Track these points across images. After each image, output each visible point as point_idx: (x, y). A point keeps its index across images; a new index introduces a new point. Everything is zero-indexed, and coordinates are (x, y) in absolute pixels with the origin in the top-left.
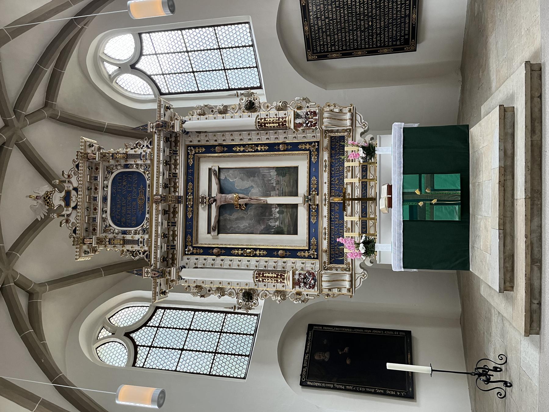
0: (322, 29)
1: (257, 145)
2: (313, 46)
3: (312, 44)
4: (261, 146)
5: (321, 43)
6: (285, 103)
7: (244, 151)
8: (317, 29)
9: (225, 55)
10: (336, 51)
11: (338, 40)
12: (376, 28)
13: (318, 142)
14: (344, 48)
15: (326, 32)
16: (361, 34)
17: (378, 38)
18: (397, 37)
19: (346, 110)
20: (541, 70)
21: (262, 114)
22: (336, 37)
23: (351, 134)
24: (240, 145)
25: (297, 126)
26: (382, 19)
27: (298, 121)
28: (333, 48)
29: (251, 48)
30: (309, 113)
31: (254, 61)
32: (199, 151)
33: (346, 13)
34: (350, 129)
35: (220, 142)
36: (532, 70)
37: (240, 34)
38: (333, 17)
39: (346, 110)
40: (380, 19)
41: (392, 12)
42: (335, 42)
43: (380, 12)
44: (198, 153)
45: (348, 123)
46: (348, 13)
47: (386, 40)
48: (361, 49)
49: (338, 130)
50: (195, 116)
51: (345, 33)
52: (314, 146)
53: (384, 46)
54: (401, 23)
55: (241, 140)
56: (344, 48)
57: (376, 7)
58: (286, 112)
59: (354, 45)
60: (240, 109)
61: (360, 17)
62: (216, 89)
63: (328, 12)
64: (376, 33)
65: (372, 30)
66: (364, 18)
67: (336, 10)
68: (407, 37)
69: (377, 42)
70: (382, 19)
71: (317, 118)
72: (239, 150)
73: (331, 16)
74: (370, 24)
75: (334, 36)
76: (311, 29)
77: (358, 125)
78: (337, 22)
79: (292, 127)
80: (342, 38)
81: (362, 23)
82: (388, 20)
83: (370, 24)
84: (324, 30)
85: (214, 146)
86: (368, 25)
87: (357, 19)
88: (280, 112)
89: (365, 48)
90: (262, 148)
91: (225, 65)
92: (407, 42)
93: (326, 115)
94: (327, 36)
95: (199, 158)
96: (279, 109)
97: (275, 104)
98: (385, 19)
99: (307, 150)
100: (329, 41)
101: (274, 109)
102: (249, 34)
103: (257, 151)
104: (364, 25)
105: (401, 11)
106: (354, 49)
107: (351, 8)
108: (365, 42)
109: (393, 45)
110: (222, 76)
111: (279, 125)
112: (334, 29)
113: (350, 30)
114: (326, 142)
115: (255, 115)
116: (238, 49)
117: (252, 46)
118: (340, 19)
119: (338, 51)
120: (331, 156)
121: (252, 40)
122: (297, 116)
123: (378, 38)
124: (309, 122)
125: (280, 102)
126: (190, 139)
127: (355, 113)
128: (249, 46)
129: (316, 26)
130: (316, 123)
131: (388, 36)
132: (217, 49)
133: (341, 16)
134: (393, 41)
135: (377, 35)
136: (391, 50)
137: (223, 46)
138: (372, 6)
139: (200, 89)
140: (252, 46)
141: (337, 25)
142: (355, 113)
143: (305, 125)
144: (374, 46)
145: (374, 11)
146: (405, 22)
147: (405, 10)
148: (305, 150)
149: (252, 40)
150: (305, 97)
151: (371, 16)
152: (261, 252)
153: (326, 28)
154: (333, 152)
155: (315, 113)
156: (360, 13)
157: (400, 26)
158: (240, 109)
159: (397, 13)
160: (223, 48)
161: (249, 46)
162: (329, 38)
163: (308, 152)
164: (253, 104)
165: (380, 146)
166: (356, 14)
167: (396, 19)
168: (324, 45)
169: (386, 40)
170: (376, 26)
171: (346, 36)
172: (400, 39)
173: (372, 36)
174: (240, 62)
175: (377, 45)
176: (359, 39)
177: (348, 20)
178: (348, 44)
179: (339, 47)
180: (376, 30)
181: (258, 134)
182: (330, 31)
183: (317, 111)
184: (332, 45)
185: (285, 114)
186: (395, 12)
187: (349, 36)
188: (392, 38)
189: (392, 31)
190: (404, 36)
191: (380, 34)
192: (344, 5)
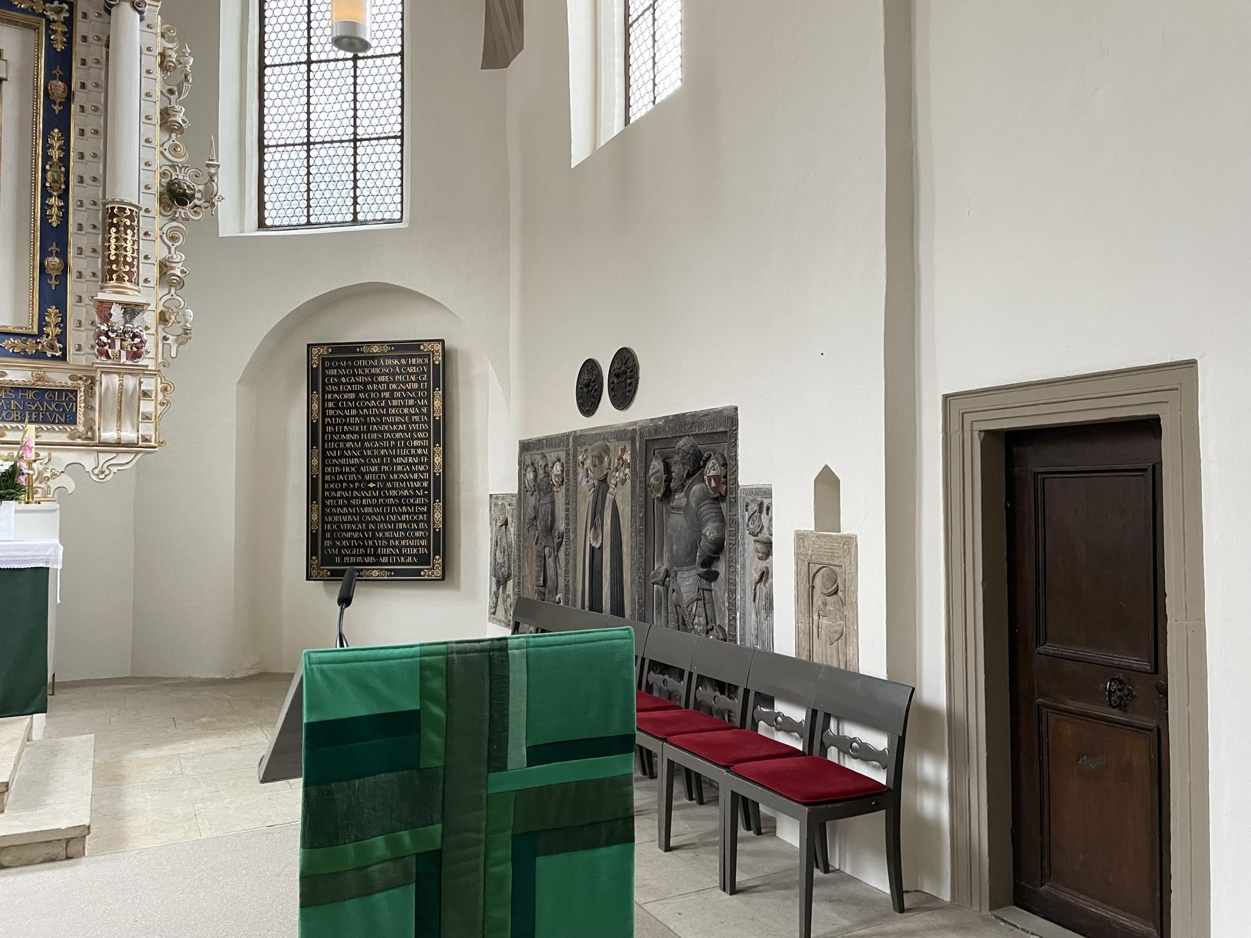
0: (372, 383)
1: (64, 196)
2: (339, 360)
3: (343, 359)
4: (60, 208)
5: (343, 380)
6: (180, 284)
7: (47, 158)
8: (373, 371)
9: (388, 149)
10: (324, 409)
11: (345, 416)
12: (361, 498)
13: (63, 358)
14: (329, 429)
15: (364, 391)
16: (353, 465)
17: (341, 502)
18: (338, 539)
19: (147, 429)
20: (68, 858)
21: (154, 222)
22: (354, 412)
23: (79, 441)
24: (66, 148)
25: (104, 309)
26: (377, 510)
27: (117, 312)
28: (331, 404)
29: (349, 218)
30: (137, 340)
31: (322, 219)
32: (55, 32)
33: (398, 436)
34: (92, 439)
35: (80, 97)
36: (68, 841)
37: (383, 198)
38: (392, 407)
39: (147, 429)
40: (377, 505)
41: (388, 530)
42: (343, 409)
43: (391, 506)
44: (48, 28)
45: (109, 435)
46: (396, 440)
47: (336, 519)
48: (324, 465)
49: (92, 408)
50: (159, 44)
51: (359, 433)
52: (52, 347)
53: (324, 514)
54: (366, 548)
55: (82, 156)
56: (329, 429)
57: (400, 497)
58: (152, 284)
59: (332, 450)
60: (173, 167)
61: (387, 464)
62: (266, 111)
63: (402, 398)
64: (352, 497)
65: (359, 489)
66: (384, 472)
67: (405, 415)
68: (338, 560)
69: (334, 498)
70: (377, 510)
71: (123, 360)
72: (52, 146)
73: (395, 403)
74: (372, 485)
75: (356, 407)
76: (373, 358)
77: (103, 458)
78: (381, 416)
79: (101, 296)
80: (350, 424)
81: (375, 469)
82: (374, 522)
83: (372, 485)
84: (369, 387)
85: (67, 79)
86: (369, 482)
87: (382, 457)
88: (156, 269)
89: (324, 474)
90: (55, 210)
91: (318, 146)
92: (327, 560)
93: (130, 382)
94: (357, 392)
95: (36, 29)
96: (164, 267)
97: (178, 257)
98: (376, 514)
99: (41, 327)
100: (345, 396)
101: (164, 253)
102: (379, 216)
103: (46, 194)
104: (370, 472)
105: (388, 546)
106: (324, 450)
107: (406, 447)
108: (335, 474)
109: (324, 531)
110: (294, 134)
111: (111, 263)
112: (368, 408)
113: (363, 441)
114: (58, 377)
115: (155, 206)
116: (350, 185)
117: (355, 221)
118: (387, 423)
119: (324, 416)
120: (16, 389)
121: (365, 222)
122: (131, 310)
123: (341, 502)
124: (113, 340)
125: (183, 272)
126: (92, 15)
127: (138, 453)
128: (355, 214)
129: (378, 370)
130: (108, 357)
131: (343, 522)
132: (355, 133)
133: (392, 424)
134: (332, 531)
135: (348, 499)
136: (314, 528)
137: (360, 151)
138: (403, 489)
139: (268, 71)
140: (355, 221)
141: (375, 416)
142: (138, 453)
143: (104, 327)
144: (327, 493)
145: (394, 493)
146: (366, 555)
147: (388, 556)
148: (42, 324)
149: (365, 222)
150: (193, 334)
151: (385, 488)
152: (57, 145)
153: (373, 391)
154: (31, 395)
155: (135, 355)
156: (392, 464)
157: (359, 546)
158: (173, 167)
159: (386, 538)
160: (308, 151)
161: (355, 214)
162: (352, 396)
163: (36, 331)
164: (183, 203)
165: (16, 511)
166: (392, 457)
167: (374, 537)
168: (338, 384)
169: (336, 519)
170: (366, 497)
171: (352, 433)
172: (334, 546)
173: (347, 489)
174: (323, 186)
175: (328, 498)
176: (343, 461)
177: (383, 440)
178: (336, 437)
179: (331, 417)
180: (357, 497)
181: (95, 203)
182: (365, 399)
183: (141, 362)
184: (336, 401)
185: (146, 280)
186: (387, 534)
187: (351, 440)
188: (339, 530)
189: (352, 530)
190: (340, 555)
191: (349, 505)
192: (412, 431)
